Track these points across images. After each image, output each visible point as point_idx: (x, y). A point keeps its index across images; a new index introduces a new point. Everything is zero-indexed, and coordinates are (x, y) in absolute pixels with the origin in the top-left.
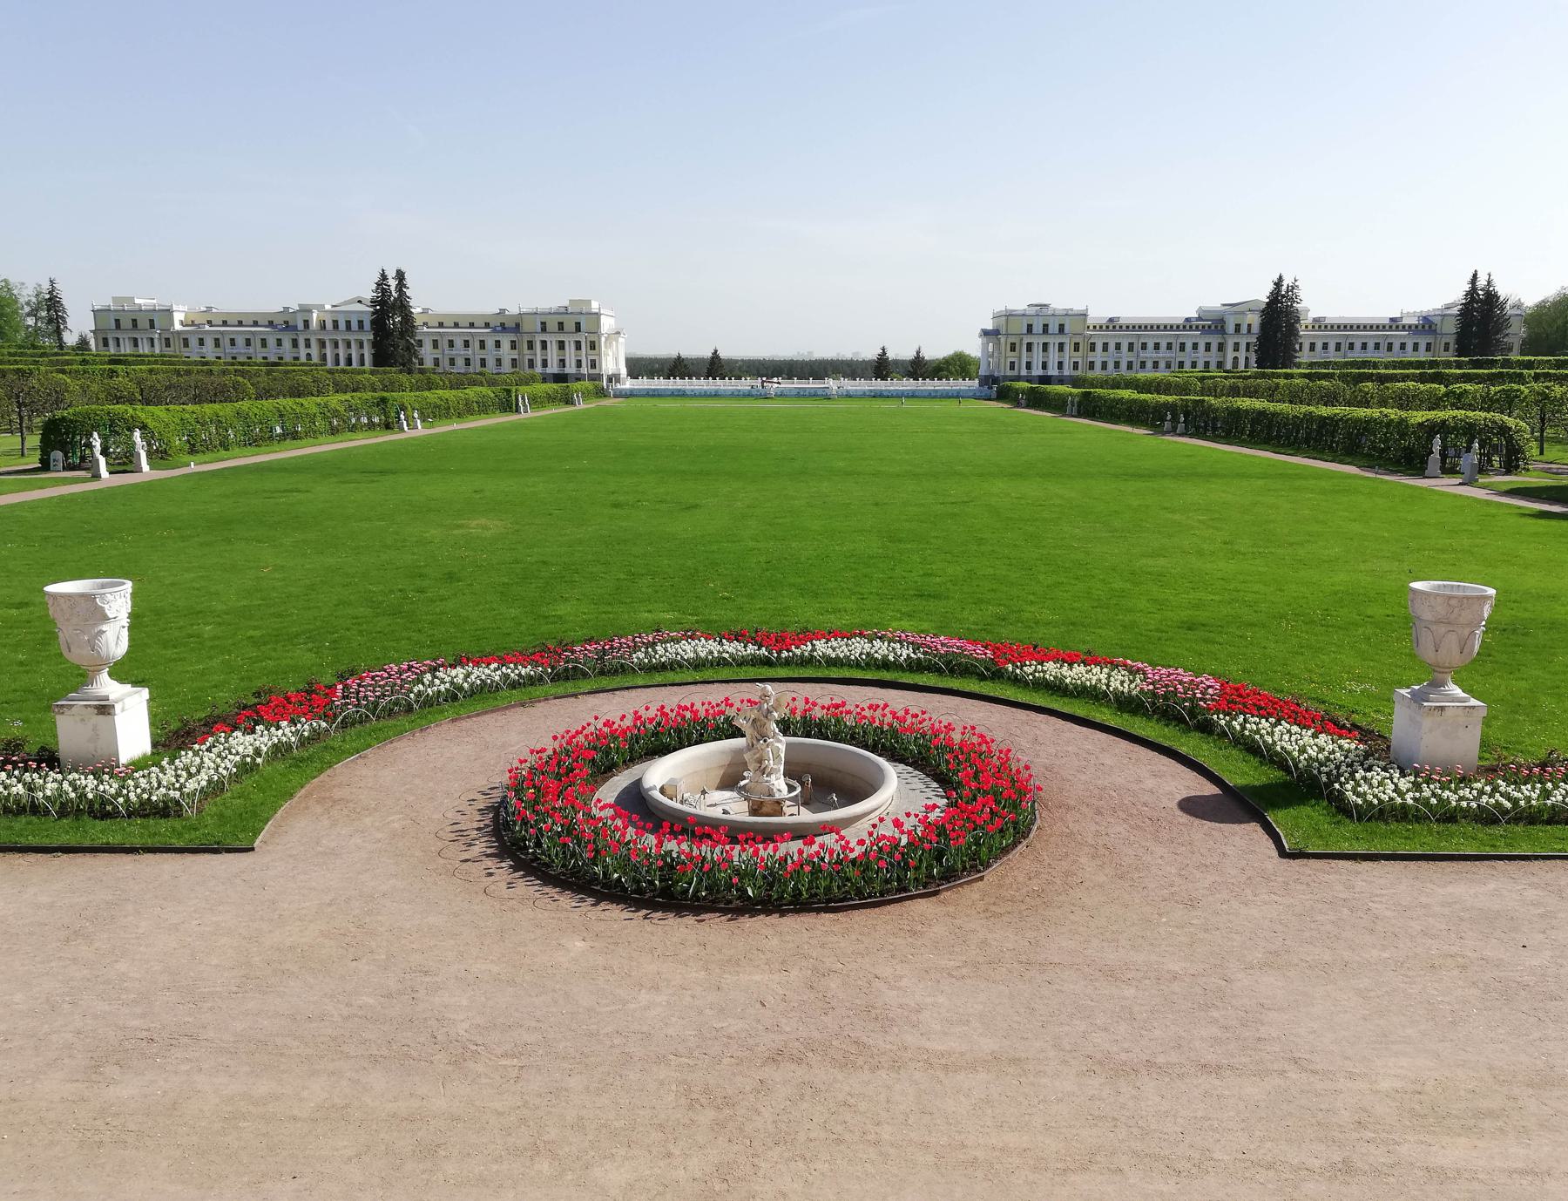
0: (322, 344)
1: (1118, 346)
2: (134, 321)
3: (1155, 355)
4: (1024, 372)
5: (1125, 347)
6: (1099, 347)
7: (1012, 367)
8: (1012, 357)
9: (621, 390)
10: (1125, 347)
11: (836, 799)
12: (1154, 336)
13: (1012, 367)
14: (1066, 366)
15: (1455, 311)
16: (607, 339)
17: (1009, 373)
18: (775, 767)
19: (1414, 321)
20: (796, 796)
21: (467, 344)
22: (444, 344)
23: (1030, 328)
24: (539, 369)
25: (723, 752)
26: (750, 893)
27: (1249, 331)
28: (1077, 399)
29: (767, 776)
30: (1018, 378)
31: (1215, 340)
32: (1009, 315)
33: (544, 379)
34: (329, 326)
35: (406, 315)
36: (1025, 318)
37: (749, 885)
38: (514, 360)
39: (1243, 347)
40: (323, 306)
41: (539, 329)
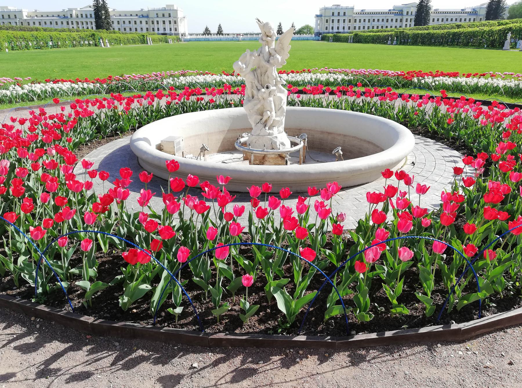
0: (78, 23)
1: (364, 20)
2: (9, 16)
3: (378, 24)
4: (331, 31)
5: (367, 21)
6: (358, 21)
7: (327, 29)
8: (327, 25)
9: (186, 39)
10: (367, 21)
11: (342, 153)
12: (377, 16)
13: (327, 29)
14: (346, 28)
15: (486, 6)
16: (180, 20)
17: (326, 31)
18: (277, 119)
19: (470, 10)
20: (298, 151)
21: (130, 22)
22: (121, 22)
23: (333, 13)
24: (156, 31)
25: (222, 119)
26: (281, 306)
27: (411, 14)
28: (352, 37)
29: (269, 129)
30: (329, 33)
31: (399, 18)
32: (326, 9)
33: (158, 34)
34: (80, 16)
35: (106, 11)
36: (331, 10)
37: (280, 287)
38: (147, 28)
39: (409, 20)
40: (77, 9)
41: (156, 16)
